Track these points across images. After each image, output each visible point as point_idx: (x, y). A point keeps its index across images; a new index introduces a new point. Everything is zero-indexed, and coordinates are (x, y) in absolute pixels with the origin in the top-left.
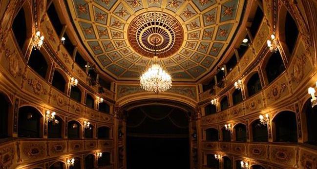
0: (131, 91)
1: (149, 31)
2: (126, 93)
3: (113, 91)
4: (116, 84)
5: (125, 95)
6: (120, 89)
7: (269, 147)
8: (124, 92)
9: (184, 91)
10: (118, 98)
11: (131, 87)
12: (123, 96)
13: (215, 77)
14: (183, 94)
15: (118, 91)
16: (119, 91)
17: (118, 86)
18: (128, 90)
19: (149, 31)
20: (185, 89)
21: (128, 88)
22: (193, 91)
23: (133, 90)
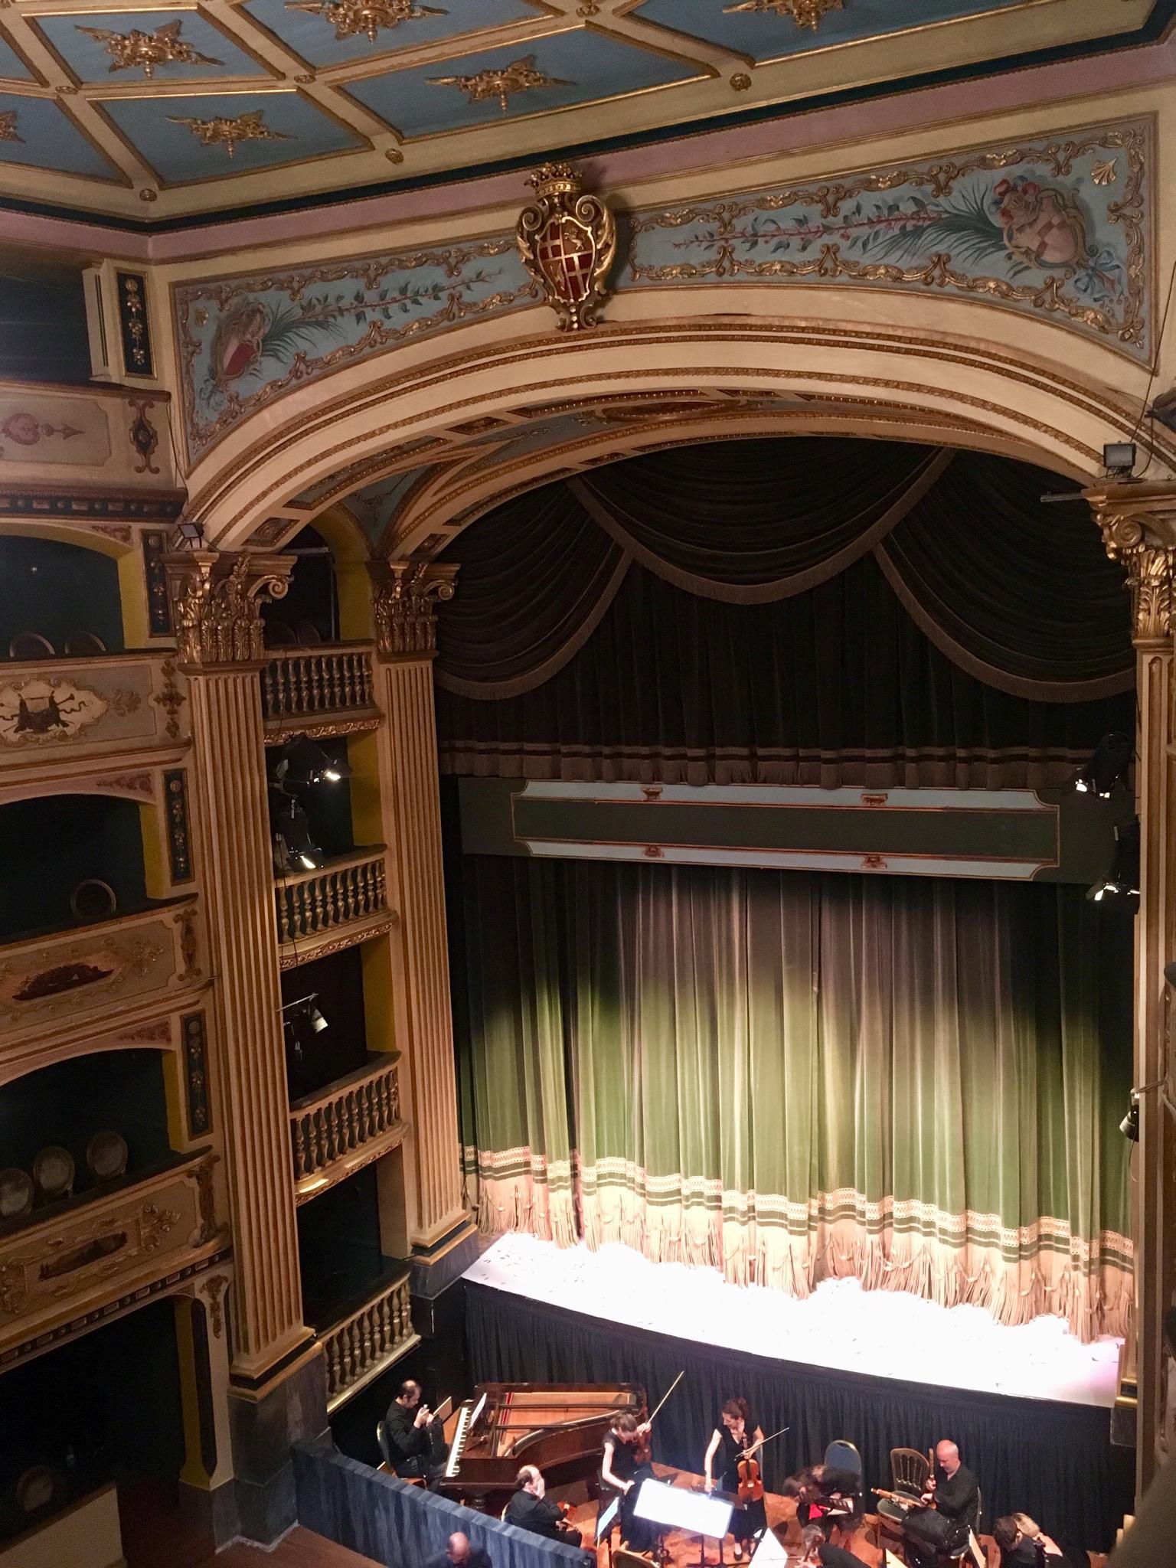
0: (321, 344)
1: (905, 1464)
2: (271, 369)
3: (114, 370)
4: (160, 281)
5: (261, 404)
6: (206, 333)
7: (941, 285)
8: (243, 360)
9: (953, 224)
10: (204, 440)
11: (313, 291)
12: (232, 420)
13: (326, 549)
14: (936, 279)
15: (185, 372)
16: (202, 363)
17: (183, 294)
18: (281, 330)
19: (905, 1464)
20: (972, 191)
21: (278, 301)
22: (1095, 195)
23: (321, 317)
